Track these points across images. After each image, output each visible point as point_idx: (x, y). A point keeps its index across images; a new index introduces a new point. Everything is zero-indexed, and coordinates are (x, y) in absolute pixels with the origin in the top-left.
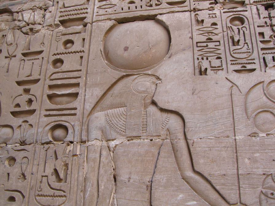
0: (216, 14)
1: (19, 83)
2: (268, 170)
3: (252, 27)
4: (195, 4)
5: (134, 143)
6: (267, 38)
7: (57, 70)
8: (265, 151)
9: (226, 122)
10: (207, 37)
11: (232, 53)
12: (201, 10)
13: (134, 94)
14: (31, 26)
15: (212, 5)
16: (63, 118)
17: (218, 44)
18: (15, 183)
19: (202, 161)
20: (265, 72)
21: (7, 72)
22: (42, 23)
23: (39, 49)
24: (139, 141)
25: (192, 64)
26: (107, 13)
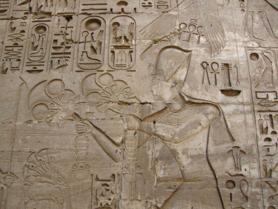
0: (26, 22)
2: (33, 149)
4: (13, 13)
6: (59, 44)
8: (35, 135)
9: (12, 111)
10: (15, 42)
11: (29, 56)
12: (16, 19)
15: (25, 15)
17: (21, 48)
20: (50, 72)
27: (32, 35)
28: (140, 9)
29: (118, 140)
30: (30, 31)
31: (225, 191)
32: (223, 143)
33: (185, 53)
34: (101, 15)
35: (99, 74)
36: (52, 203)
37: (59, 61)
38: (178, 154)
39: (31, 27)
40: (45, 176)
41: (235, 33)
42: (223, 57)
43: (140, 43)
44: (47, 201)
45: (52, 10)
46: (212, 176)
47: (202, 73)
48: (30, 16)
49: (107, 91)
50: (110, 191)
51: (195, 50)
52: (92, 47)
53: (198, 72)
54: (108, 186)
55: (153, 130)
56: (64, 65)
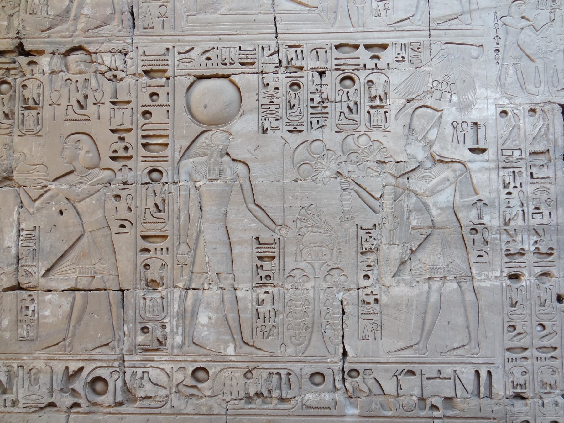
1: (113, 131)
3: (306, 92)
5: (213, 184)
6: (316, 104)
7: (147, 121)
13: (213, 147)
14: (114, 73)
15: (277, 69)
17: (278, 107)
18: (123, 214)
19: (260, 197)
21: (99, 119)
22: (125, 70)
23: (127, 99)
24: (217, 182)
25: (257, 122)
26: (186, 68)
27: (287, 92)
28: (394, 65)
29: (378, 196)
30: (284, 87)
31: (469, 237)
32: (469, 196)
33: (437, 112)
34: (354, 72)
35: (357, 135)
36: (324, 249)
37: (318, 121)
38: (429, 206)
39: (285, 83)
40: (315, 227)
41: (487, 89)
42: (474, 116)
43: (394, 103)
44: (320, 248)
45: (303, 64)
46: (458, 225)
47: (452, 132)
48: (282, 69)
49: (366, 151)
50: (373, 238)
51: (447, 109)
52: (349, 107)
53: (449, 130)
54: (370, 233)
55: (408, 185)
56: (323, 126)
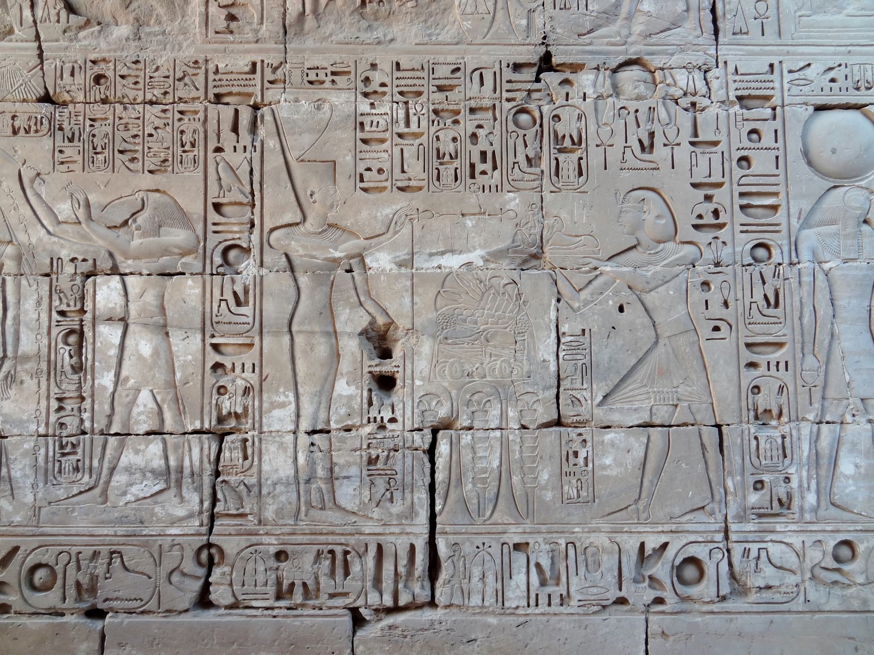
1: (695, 185)
16: (767, 235)
23: (715, 139)
26: (802, 93)
